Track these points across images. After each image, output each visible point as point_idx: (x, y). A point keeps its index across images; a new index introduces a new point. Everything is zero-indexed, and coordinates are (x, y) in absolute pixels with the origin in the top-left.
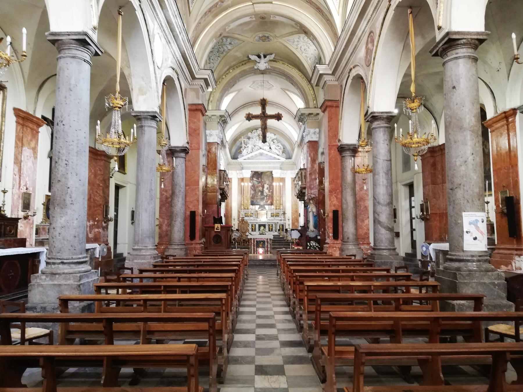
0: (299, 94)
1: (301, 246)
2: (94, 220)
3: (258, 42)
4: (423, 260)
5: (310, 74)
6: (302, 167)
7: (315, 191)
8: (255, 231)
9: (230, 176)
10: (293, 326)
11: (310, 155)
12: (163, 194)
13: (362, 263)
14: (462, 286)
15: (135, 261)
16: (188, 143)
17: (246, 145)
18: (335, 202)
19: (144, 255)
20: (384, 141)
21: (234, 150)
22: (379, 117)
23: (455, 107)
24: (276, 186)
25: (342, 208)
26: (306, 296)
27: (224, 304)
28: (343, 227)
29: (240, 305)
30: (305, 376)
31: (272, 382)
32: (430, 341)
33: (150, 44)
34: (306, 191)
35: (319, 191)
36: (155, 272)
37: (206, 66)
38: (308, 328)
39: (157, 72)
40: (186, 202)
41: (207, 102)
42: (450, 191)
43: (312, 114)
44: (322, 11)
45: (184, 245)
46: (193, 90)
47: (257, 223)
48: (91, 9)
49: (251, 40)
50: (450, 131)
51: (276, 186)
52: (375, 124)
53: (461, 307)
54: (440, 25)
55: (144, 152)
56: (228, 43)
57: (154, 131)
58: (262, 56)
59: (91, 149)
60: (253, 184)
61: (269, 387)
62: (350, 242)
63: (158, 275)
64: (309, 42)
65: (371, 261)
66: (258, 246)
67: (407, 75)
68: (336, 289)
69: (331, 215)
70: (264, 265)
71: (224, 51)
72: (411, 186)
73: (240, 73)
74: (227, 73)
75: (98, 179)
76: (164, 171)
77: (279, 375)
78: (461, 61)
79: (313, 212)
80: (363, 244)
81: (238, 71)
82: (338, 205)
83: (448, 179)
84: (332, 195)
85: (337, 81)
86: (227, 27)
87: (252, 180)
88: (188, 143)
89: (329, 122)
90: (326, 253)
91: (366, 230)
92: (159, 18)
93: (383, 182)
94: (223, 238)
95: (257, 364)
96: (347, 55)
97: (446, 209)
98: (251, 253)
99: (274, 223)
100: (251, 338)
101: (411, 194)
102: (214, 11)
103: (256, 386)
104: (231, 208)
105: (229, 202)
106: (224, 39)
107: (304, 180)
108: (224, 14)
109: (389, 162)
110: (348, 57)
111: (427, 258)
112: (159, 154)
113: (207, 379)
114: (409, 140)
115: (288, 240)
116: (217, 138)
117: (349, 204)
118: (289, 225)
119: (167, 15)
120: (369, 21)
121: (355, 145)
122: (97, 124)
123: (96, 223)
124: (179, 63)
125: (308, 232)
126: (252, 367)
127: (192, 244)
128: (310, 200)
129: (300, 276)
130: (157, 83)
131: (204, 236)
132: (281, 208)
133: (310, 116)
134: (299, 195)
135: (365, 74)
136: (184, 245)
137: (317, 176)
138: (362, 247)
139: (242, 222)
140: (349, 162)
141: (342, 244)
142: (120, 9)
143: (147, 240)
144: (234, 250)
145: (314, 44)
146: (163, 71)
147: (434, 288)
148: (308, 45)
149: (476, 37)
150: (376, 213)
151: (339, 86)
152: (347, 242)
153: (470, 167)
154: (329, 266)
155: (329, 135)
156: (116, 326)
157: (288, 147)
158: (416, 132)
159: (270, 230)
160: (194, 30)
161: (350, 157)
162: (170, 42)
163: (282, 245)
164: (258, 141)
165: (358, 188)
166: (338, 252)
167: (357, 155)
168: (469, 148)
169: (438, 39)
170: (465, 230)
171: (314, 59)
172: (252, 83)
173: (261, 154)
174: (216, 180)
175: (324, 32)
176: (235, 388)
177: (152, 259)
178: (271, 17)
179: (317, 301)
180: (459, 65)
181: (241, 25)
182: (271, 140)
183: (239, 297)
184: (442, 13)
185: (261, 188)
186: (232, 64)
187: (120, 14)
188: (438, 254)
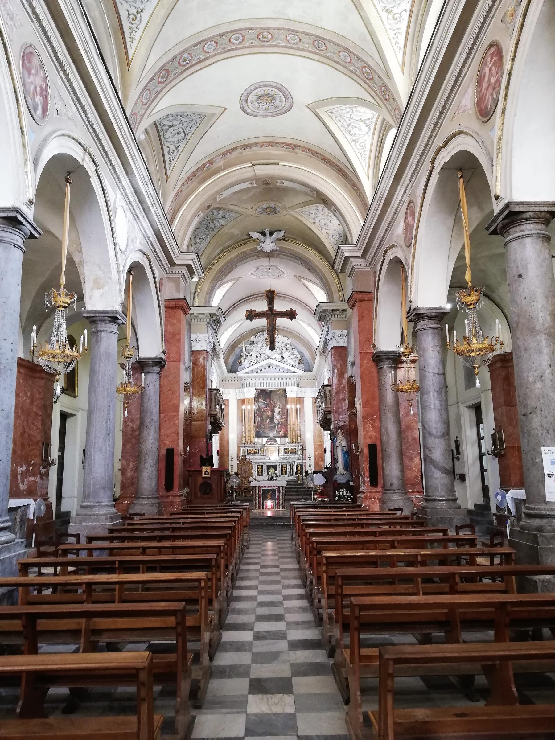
0: (319, 284)
1: (326, 496)
2: (29, 465)
3: (262, 216)
4: (498, 514)
5: (333, 255)
6: (326, 383)
8: (262, 475)
9: (224, 397)
10: (309, 617)
11: (336, 366)
12: (128, 425)
13: (410, 520)
14: (545, 553)
15: (84, 524)
17: (249, 353)
18: (372, 433)
19: (97, 515)
20: (433, 347)
21: (231, 360)
23: (524, 302)
26: (324, 572)
27: (203, 588)
28: (383, 468)
29: (234, 587)
30: (320, 695)
32: (498, 639)
33: (110, 221)
34: (332, 417)
35: (349, 416)
36: (111, 539)
37: (190, 247)
38: (328, 621)
39: (119, 258)
41: (192, 296)
43: (337, 310)
44: (345, 173)
47: (264, 463)
48: (26, 177)
49: (252, 213)
50: (518, 334)
52: (421, 324)
53: (546, 584)
54: (498, 194)
56: (221, 217)
57: (115, 338)
58: (268, 233)
60: (259, 407)
61: (269, 712)
63: (116, 544)
65: (422, 518)
66: (265, 498)
67: (461, 257)
68: (372, 562)
69: (366, 451)
71: (215, 227)
72: (477, 408)
73: (237, 256)
74: (219, 256)
75: (36, 406)
77: (283, 693)
78: (528, 241)
80: (413, 492)
81: (235, 253)
82: (376, 437)
83: (519, 401)
84: (367, 424)
85: (369, 266)
86: (217, 196)
87: (258, 401)
88: (164, 352)
90: (360, 506)
92: (123, 187)
93: (435, 404)
94: (214, 486)
95: (252, 676)
96: (381, 231)
98: (255, 508)
99: (289, 462)
100: (247, 636)
101: (479, 420)
102: (200, 175)
103: (249, 711)
104: (228, 442)
105: (225, 433)
106: (215, 212)
107: (328, 400)
108: (213, 179)
109: (442, 376)
110: (382, 235)
112: (123, 368)
113: (172, 702)
114: (465, 347)
115: (309, 488)
116: (205, 344)
117: (391, 435)
118: (310, 465)
119: (134, 182)
120: (407, 188)
122: (32, 331)
123: (31, 468)
124: (152, 244)
125: (335, 476)
127: (169, 496)
128: (337, 429)
129: (318, 543)
130: (119, 272)
131: (186, 483)
132: (299, 440)
133: (335, 313)
134: (323, 421)
135: (405, 256)
136: (158, 498)
139: (243, 461)
140: (389, 376)
141: (383, 493)
142: (68, 175)
143: (102, 493)
146: (129, 255)
149: (546, 209)
150: (427, 448)
151: (372, 273)
153: (549, 383)
154: (362, 526)
155: (360, 339)
156: (42, 624)
157: (307, 355)
159: (284, 473)
162: (138, 218)
163: (301, 495)
164: (265, 347)
165: (402, 412)
167: (399, 366)
168: (546, 357)
169: (496, 212)
170: (546, 472)
171: (338, 236)
172: (254, 269)
173: (270, 366)
174: (204, 403)
177: (108, 521)
179: (338, 580)
180: (525, 246)
181: (235, 193)
182: (283, 345)
183: (232, 574)
184: (499, 178)
185: (270, 413)
186: (228, 244)
187: (67, 181)
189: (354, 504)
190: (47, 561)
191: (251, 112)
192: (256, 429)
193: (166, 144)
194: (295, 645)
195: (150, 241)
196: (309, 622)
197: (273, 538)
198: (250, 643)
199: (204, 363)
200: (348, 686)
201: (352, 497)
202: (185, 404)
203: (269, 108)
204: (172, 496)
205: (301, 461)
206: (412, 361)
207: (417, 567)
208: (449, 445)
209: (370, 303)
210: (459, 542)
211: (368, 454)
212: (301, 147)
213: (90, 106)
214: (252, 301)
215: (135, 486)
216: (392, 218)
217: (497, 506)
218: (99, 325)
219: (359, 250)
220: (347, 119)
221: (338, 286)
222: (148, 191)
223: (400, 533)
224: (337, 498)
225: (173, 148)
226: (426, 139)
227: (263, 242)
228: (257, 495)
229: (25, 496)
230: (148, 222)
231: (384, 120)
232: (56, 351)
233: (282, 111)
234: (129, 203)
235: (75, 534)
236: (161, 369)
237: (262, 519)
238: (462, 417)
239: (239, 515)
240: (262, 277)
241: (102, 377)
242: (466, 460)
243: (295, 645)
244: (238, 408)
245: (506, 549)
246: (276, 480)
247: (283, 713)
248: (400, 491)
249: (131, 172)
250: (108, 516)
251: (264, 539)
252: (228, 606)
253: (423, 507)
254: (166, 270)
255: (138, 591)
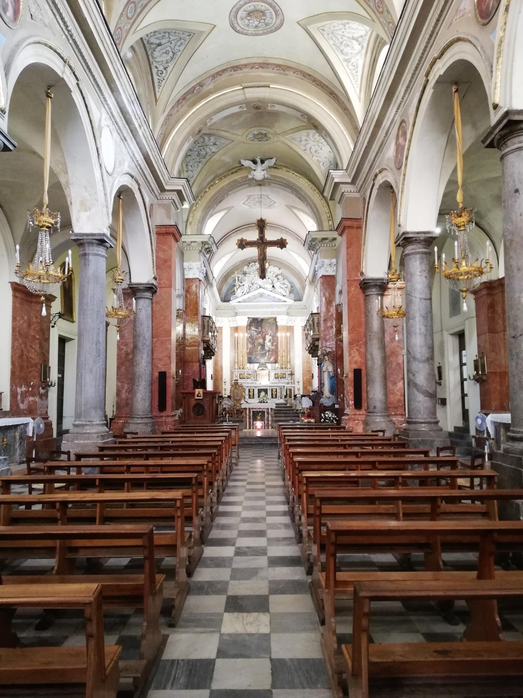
0: (311, 214)
1: (313, 417)
2: (28, 386)
3: (253, 142)
4: (478, 436)
6: (315, 311)
7: (331, 343)
8: (253, 397)
9: (218, 325)
10: (290, 533)
11: (324, 294)
12: (122, 349)
13: (392, 442)
15: (76, 442)
16: (155, 278)
17: (241, 283)
18: (357, 358)
19: (89, 433)
20: (420, 272)
21: (224, 290)
22: (414, 239)
23: (519, 219)
24: (282, 337)
25: (366, 366)
26: (305, 492)
27: (178, 508)
28: (367, 392)
29: (219, 502)
31: (247, 624)
33: (95, 140)
34: (320, 344)
35: (336, 343)
36: (101, 457)
40: (152, 359)
42: (512, 340)
43: (326, 239)
44: (336, 95)
45: (151, 418)
46: (164, 206)
47: (255, 387)
50: (512, 254)
51: (282, 337)
52: (410, 249)
55: (88, 290)
56: (212, 144)
58: (259, 161)
59: (15, 286)
60: (251, 335)
62: (377, 413)
63: (107, 462)
64: (321, 141)
65: (404, 439)
66: (255, 419)
67: (452, 182)
68: (354, 482)
69: (351, 376)
70: (263, 445)
71: (206, 154)
72: (461, 336)
73: (229, 184)
74: (211, 184)
75: (33, 330)
76: (121, 317)
77: (259, 612)
79: (329, 372)
80: (396, 415)
81: (226, 182)
83: (509, 323)
84: (353, 349)
86: (208, 121)
87: (250, 329)
88: (155, 278)
89: (347, 248)
90: (344, 428)
91: (399, 396)
92: (108, 105)
93: (420, 329)
94: (206, 408)
95: (230, 593)
96: (372, 155)
97: (507, 367)
98: (246, 428)
99: (279, 386)
100: (227, 551)
101: (462, 347)
102: (190, 98)
104: (222, 367)
105: (219, 359)
106: (206, 138)
108: (204, 102)
109: (429, 301)
110: (372, 159)
111: (484, 435)
114: (454, 269)
115: (297, 410)
116: (198, 273)
117: (375, 361)
118: (299, 390)
119: (119, 101)
120: (399, 106)
121: (383, 279)
123: (30, 389)
124: (141, 168)
125: (322, 399)
126: (222, 599)
127: (162, 417)
128: (325, 355)
129: (300, 463)
130: (105, 194)
131: (178, 404)
132: (289, 366)
133: (324, 241)
134: (311, 348)
136: (151, 418)
137: (334, 323)
138: (394, 419)
139: (235, 385)
140: (376, 303)
141: (367, 416)
142: (49, 89)
143: (93, 413)
144: (225, 424)
145: (328, 144)
146: (116, 178)
147: (490, 479)
148: (320, 145)
151: (361, 199)
152: (372, 413)
154: (344, 446)
157: (298, 285)
158: (465, 257)
159: (274, 396)
160: (162, 125)
161: (376, 296)
162: (125, 139)
163: (289, 417)
165: (387, 339)
166: (362, 426)
167: (386, 293)
171: (329, 164)
172: (246, 198)
173: (261, 295)
174: (197, 330)
175: (340, 125)
176: (192, 635)
178: (268, 106)
182: (274, 276)
183: (218, 491)
184: (499, 84)
185: (261, 341)
187: (48, 96)
188: (498, 428)
189: (338, 425)
190: (28, 479)
191: (241, 30)
192: (247, 355)
193: (155, 64)
194: (275, 562)
195: (139, 165)
196: (291, 538)
197: (261, 456)
198: (231, 559)
199: (196, 290)
200: (323, 607)
201: (337, 419)
202: (177, 329)
203: (260, 25)
204: (165, 416)
205: (290, 385)
206: (399, 289)
207: (398, 489)
208: (432, 370)
209: (359, 230)
210: (440, 464)
211: (353, 379)
212: (293, 68)
213: (68, 12)
214: (244, 231)
215: (130, 406)
216: (383, 141)
217: (476, 429)
218: (87, 248)
219: (349, 176)
220: (339, 37)
221: (328, 215)
222: (134, 111)
223: (381, 454)
224: (323, 420)
225: (161, 68)
226: (421, 51)
227: (255, 170)
228: (248, 417)
229: (25, 415)
230: (136, 144)
231: (378, 36)
232: (40, 272)
233: (273, 28)
234: (115, 123)
235: (66, 451)
236: (153, 294)
237: (251, 438)
238: (445, 345)
239: (227, 434)
240: (253, 207)
241: (91, 300)
242: (447, 385)
243: (275, 562)
244: (231, 336)
245: (488, 471)
246: (267, 402)
247: (257, 634)
248: (383, 414)
249: (116, 89)
250: (100, 435)
251: (252, 457)
252: (212, 521)
253: (405, 430)
254: (156, 196)
255: (123, 508)
